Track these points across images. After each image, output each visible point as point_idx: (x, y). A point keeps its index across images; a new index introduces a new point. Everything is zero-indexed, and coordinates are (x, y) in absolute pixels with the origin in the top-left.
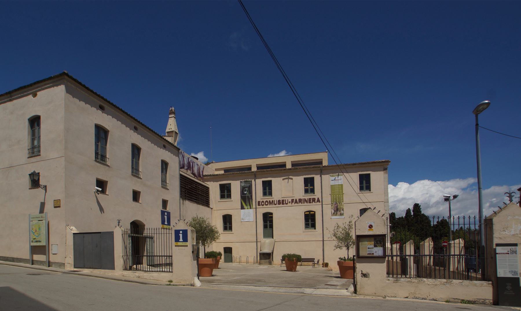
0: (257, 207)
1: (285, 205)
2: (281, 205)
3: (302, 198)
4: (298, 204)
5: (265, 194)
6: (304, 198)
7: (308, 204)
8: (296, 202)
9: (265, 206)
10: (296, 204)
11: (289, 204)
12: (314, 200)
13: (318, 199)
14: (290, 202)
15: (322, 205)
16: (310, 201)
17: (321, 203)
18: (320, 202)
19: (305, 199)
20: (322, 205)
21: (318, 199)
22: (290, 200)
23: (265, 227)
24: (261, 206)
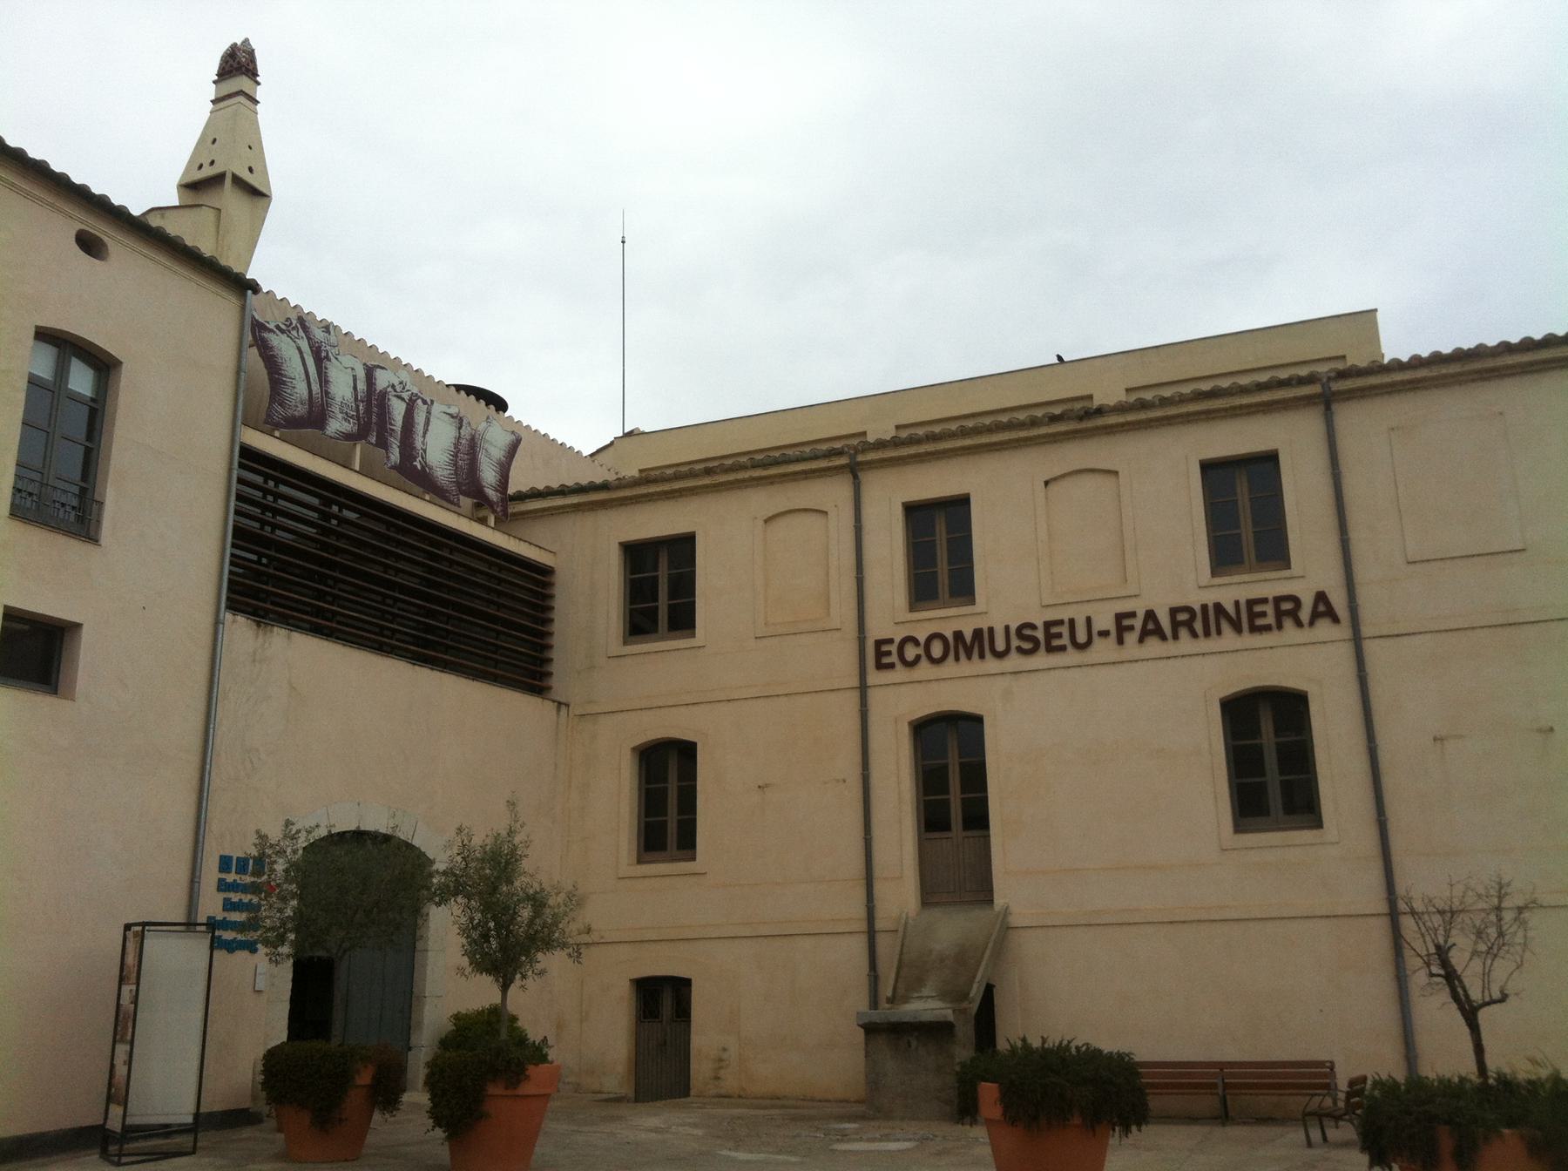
0: (874, 677)
1: (1072, 657)
2: (1041, 660)
3: (1195, 599)
4: (1170, 648)
5: (922, 591)
6: (1210, 597)
7: (1249, 640)
11: (1103, 649)
12: (1287, 610)
13: (1321, 597)
14: (1104, 634)
16: (1249, 618)
18: (1336, 620)
19: (1219, 607)
20: (1357, 640)
21: (1321, 597)
22: (1104, 621)
24: (900, 674)
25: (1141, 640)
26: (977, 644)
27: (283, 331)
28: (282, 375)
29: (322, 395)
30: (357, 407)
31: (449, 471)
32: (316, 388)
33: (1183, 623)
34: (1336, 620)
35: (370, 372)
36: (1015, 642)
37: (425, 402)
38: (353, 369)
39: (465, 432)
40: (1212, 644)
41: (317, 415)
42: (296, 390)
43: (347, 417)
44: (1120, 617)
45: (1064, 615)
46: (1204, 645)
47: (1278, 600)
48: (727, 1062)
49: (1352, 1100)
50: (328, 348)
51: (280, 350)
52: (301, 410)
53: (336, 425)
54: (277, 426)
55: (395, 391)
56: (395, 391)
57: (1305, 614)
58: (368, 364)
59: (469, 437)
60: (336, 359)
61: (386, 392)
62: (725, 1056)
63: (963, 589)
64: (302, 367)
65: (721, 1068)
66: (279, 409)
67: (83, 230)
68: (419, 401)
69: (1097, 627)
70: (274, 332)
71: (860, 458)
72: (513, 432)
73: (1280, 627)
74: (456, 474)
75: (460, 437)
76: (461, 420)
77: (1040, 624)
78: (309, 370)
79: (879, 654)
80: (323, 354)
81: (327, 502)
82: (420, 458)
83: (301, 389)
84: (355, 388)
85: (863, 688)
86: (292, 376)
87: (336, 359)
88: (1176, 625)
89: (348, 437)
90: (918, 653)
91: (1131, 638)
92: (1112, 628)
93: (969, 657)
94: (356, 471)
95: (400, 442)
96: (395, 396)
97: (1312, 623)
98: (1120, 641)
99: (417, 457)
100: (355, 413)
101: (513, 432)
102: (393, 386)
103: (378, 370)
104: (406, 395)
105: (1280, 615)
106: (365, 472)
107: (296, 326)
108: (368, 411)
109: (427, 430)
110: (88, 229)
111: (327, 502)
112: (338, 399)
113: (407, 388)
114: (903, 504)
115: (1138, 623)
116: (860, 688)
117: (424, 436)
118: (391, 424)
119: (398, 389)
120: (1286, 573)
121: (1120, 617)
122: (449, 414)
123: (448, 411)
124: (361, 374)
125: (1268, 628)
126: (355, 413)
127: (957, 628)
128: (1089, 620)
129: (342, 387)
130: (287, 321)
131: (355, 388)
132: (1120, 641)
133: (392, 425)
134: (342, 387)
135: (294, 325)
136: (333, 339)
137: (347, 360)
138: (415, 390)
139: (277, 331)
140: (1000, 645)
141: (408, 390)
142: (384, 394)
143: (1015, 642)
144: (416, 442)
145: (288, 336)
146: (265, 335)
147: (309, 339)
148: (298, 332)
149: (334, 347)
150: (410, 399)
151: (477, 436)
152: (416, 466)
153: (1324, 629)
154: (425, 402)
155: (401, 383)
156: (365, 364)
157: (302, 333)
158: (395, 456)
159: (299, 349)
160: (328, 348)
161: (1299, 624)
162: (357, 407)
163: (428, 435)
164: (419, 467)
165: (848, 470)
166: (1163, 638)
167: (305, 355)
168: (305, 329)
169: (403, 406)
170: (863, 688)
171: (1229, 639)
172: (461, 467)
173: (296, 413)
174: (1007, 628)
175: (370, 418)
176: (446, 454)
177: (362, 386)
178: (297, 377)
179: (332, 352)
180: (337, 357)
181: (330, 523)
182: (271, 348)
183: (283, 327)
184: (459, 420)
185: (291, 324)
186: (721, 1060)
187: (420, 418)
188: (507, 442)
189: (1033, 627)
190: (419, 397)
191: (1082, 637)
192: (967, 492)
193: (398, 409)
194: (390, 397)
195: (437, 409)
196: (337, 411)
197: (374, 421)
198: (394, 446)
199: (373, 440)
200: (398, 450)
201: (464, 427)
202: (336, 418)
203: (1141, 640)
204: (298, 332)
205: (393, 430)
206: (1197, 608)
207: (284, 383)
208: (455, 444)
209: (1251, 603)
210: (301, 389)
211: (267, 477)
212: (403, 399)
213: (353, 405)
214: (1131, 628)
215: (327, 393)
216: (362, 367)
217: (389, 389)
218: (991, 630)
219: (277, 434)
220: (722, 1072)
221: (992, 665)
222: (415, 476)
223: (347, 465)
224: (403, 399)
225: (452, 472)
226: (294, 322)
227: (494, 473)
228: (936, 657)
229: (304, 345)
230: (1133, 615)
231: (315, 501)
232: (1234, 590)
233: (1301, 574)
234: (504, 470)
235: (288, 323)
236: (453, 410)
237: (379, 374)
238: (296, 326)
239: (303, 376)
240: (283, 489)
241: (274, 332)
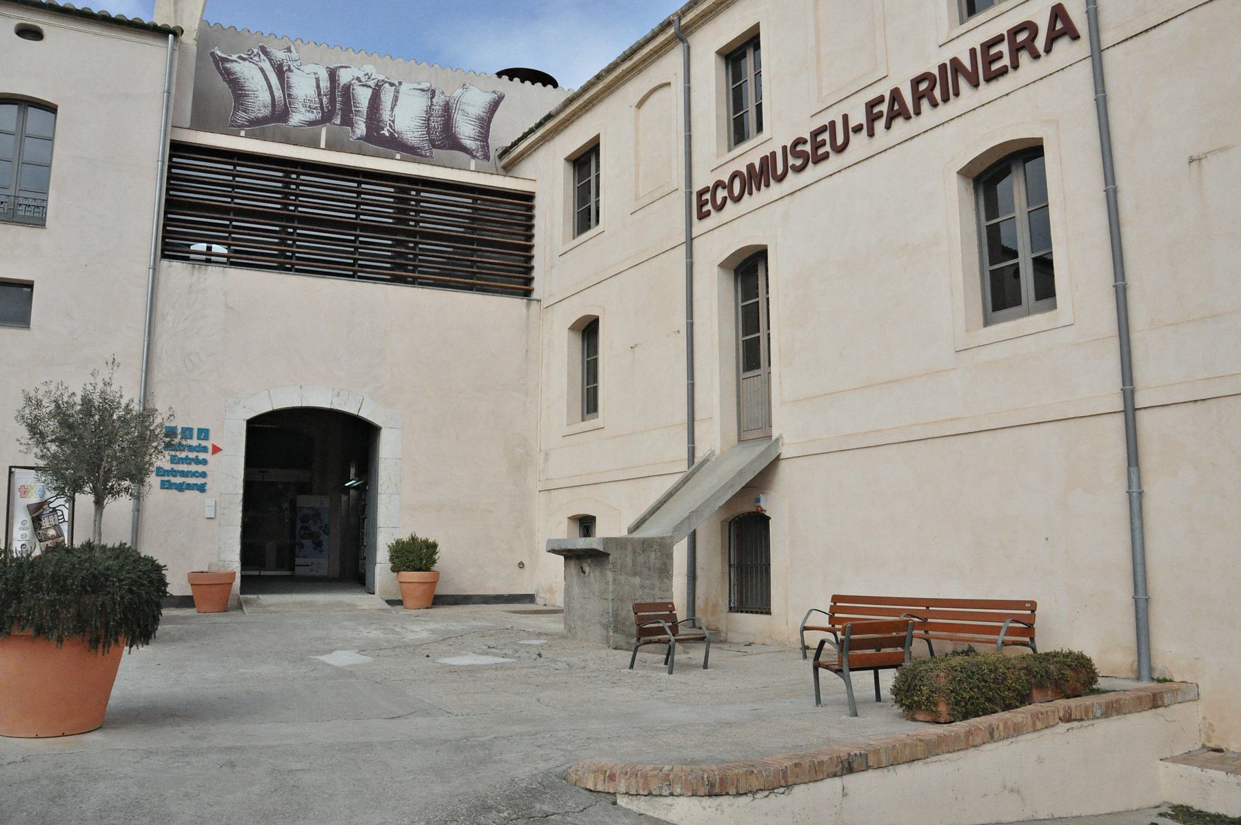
4: (916, 124)
7: (988, 91)
11: (859, 142)
13: (1058, 13)
14: (858, 129)
17: (1081, 48)
18: (1076, 37)
22: (858, 117)
25: (888, 127)
27: (244, 59)
28: (245, 90)
29: (285, 98)
30: (321, 101)
31: (420, 133)
32: (278, 93)
34: (1076, 37)
36: (791, 161)
37: (392, 85)
39: (439, 100)
41: (280, 113)
42: (258, 99)
45: (823, 120)
46: (945, 111)
47: (1015, 32)
49: (836, 615)
50: (289, 63)
52: (266, 112)
53: (296, 119)
54: (242, 126)
55: (360, 81)
57: (1040, 43)
58: (331, 67)
60: (299, 69)
61: (351, 84)
64: (265, 82)
67: (21, 24)
68: (387, 85)
69: (853, 123)
71: (683, 22)
72: (494, 92)
73: (1016, 66)
74: (428, 133)
75: (432, 105)
77: (808, 137)
79: (701, 204)
80: (285, 68)
81: (288, 174)
82: (388, 128)
83: (265, 97)
84: (318, 87)
88: (918, 98)
89: (312, 123)
90: (723, 196)
91: (880, 125)
93: (759, 189)
94: (323, 149)
97: (1048, 50)
102: (358, 79)
103: (342, 70)
104: (372, 83)
105: (1016, 50)
106: (330, 147)
108: (332, 101)
110: (24, 22)
111: (288, 174)
112: (301, 97)
113: (373, 77)
115: (884, 107)
117: (392, 109)
122: (419, 89)
123: (420, 87)
125: (1003, 72)
128: (845, 117)
131: (318, 87)
132: (871, 134)
135: (255, 53)
138: (381, 77)
139: (240, 61)
142: (347, 89)
143: (791, 161)
144: (384, 116)
145: (250, 62)
146: (228, 65)
147: (270, 60)
148: (259, 57)
150: (377, 85)
151: (452, 101)
154: (392, 85)
156: (327, 68)
157: (263, 56)
158: (361, 129)
159: (262, 70)
161: (1036, 56)
162: (321, 101)
163: (396, 109)
164: (387, 134)
165: (678, 40)
167: (267, 73)
169: (369, 92)
171: (968, 96)
172: (434, 128)
174: (784, 148)
176: (417, 120)
177: (325, 84)
178: (260, 88)
180: (300, 67)
181: (410, 194)
182: (234, 73)
190: (386, 82)
193: (363, 97)
194: (355, 87)
199: (338, 121)
201: (436, 97)
202: (300, 112)
203: (888, 127)
204: (259, 57)
206: (936, 72)
207: (247, 96)
209: (987, 46)
212: (369, 87)
213: (317, 99)
214: (880, 115)
215: (290, 95)
217: (354, 81)
219: (243, 133)
222: (395, 145)
223: (315, 145)
224: (369, 87)
229: (266, 65)
234: (485, 124)
236: (425, 86)
238: (258, 53)
239: (266, 87)
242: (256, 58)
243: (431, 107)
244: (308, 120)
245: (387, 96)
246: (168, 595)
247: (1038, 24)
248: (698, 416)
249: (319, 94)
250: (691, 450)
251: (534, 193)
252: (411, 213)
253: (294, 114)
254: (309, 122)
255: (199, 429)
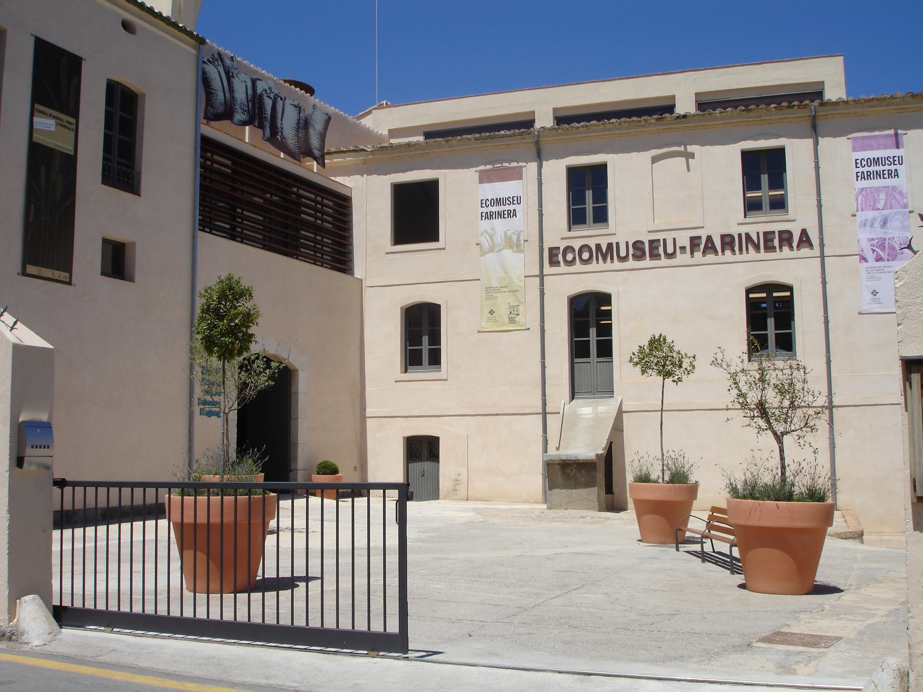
0: (547, 269)
1: (664, 261)
2: (647, 262)
3: (734, 230)
4: (720, 258)
5: (576, 218)
6: (743, 230)
7: (763, 254)
8: (710, 247)
9: (578, 266)
10: (710, 257)
11: (681, 258)
12: (786, 238)
13: (804, 232)
14: (683, 248)
15: (822, 257)
16: (768, 242)
18: (811, 245)
19: (748, 236)
20: (822, 257)
21: (804, 232)
22: (684, 240)
23: (579, 350)
24: (563, 268)
25: (704, 253)
26: (608, 252)
27: (210, 62)
30: (248, 104)
32: (228, 95)
33: (727, 244)
34: (811, 245)
35: (254, 82)
38: (245, 82)
40: (745, 257)
43: (244, 111)
44: (692, 239)
46: (738, 257)
47: (781, 233)
48: (461, 482)
50: (233, 70)
51: (210, 74)
55: (267, 93)
56: (267, 93)
59: (304, 119)
60: (237, 76)
62: (459, 478)
63: (601, 216)
65: (458, 484)
66: (211, 109)
68: (279, 98)
70: (207, 64)
76: (300, 108)
78: (224, 84)
80: (231, 74)
82: (280, 134)
83: (221, 96)
85: (542, 276)
86: (216, 89)
87: (237, 76)
92: (687, 245)
95: (270, 124)
96: (267, 96)
98: (692, 253)
99: (278, 133)
100: (247, 109)
101: (327, 114)
102: (266, 91)
103: (258, 81)
104: (272, 96)
107: (217, 59)
109: (283, 116)
112: (239, 101)
113: (273, 91)
114: (566, 166)
116: (834, 407)
117: (282, 120)
118: (265, 114)
119: (268, 92)
120: (786, 218)
121: (692, 239)
122: (294, 105)
124: (249, 84)
126: (247, 109)
127: (598, 242)
129: (240, 95)
130: (212, 56)
133: (266, 114)
134: (240, 95)
135: (216, 58)
136: (235, 64)
137: (242, 76)
138: (277, 92)
140: (623, 253)
141: (273, 93)
142: (261, 96)
149: (236, 69)
152: (278, 138)
153: (805, 251)
154: (281, 99)
155: (269, 88)
156: (251, 79)
159: (219, 72)
160: (233, 70)
161: (791, 247)
162: (248, 104)
166: (716, 252)
168: (222, 60)
170: (542, 276)
173: (219, 111)
175: (255, 111)
177: (250, 92)
179: (235, 72)
180: (238, 75)
183: (211, 60)
184: (299, 108)
185: (215, 57)
186: (457, 480)
187: (279, 109)
188: (324, 120)
189: (642, 243)
191: (670, 250)
192: (605, 161)
193: (268, 103)
195: (288, 102)
196: (238, 108)
197: (257, 112)
198: (267, 127)
199: (257, 124)
200: (269, 129)
202: (238, 113)
205: (266, 117)
208: (297, 123)
210: (221, 96)
211: (316, 195)
212: (271, 98)
215: (233, 97)
216: (250, 80)
217: (264, 92)
218: (618, 244)
220: (458, 487)
221: (617, 265)
224: (271, 98)
225: (296, 141)
226: (216, 56)
227: (317, 140)
228: (584, 259)
230: (699, 238)
231: (229, 162)
232: (760, 224)
233: (794, 219)
235: (213, 57)
237: (259, 83)
239: (221, 88)
240: (216, 157)
241: (207, 64)
242: (216, 63)
243: (299, 120)
244: (242, 120)
245: (280, 103)
246: (508, 248)
247: (793, 232)
248: (94, 574)
249: (247, 100)
250: (541, 248)
251: (650, 260)
252: (293, 196)
253: (235, 113)
254: (244, 122)
255: (779, 231)
